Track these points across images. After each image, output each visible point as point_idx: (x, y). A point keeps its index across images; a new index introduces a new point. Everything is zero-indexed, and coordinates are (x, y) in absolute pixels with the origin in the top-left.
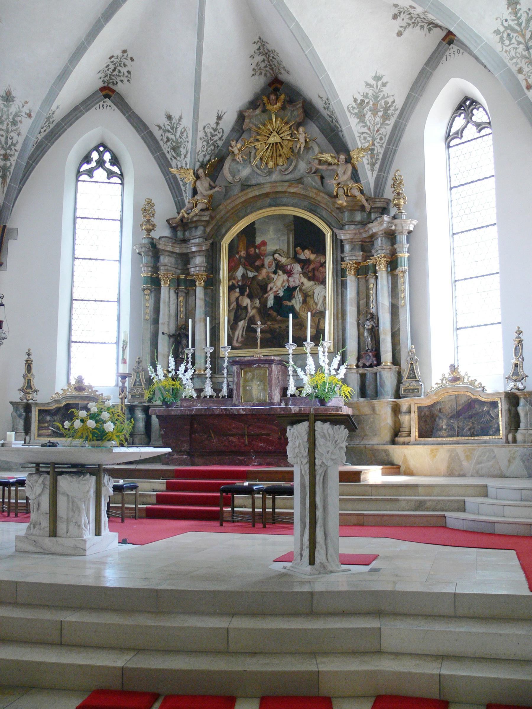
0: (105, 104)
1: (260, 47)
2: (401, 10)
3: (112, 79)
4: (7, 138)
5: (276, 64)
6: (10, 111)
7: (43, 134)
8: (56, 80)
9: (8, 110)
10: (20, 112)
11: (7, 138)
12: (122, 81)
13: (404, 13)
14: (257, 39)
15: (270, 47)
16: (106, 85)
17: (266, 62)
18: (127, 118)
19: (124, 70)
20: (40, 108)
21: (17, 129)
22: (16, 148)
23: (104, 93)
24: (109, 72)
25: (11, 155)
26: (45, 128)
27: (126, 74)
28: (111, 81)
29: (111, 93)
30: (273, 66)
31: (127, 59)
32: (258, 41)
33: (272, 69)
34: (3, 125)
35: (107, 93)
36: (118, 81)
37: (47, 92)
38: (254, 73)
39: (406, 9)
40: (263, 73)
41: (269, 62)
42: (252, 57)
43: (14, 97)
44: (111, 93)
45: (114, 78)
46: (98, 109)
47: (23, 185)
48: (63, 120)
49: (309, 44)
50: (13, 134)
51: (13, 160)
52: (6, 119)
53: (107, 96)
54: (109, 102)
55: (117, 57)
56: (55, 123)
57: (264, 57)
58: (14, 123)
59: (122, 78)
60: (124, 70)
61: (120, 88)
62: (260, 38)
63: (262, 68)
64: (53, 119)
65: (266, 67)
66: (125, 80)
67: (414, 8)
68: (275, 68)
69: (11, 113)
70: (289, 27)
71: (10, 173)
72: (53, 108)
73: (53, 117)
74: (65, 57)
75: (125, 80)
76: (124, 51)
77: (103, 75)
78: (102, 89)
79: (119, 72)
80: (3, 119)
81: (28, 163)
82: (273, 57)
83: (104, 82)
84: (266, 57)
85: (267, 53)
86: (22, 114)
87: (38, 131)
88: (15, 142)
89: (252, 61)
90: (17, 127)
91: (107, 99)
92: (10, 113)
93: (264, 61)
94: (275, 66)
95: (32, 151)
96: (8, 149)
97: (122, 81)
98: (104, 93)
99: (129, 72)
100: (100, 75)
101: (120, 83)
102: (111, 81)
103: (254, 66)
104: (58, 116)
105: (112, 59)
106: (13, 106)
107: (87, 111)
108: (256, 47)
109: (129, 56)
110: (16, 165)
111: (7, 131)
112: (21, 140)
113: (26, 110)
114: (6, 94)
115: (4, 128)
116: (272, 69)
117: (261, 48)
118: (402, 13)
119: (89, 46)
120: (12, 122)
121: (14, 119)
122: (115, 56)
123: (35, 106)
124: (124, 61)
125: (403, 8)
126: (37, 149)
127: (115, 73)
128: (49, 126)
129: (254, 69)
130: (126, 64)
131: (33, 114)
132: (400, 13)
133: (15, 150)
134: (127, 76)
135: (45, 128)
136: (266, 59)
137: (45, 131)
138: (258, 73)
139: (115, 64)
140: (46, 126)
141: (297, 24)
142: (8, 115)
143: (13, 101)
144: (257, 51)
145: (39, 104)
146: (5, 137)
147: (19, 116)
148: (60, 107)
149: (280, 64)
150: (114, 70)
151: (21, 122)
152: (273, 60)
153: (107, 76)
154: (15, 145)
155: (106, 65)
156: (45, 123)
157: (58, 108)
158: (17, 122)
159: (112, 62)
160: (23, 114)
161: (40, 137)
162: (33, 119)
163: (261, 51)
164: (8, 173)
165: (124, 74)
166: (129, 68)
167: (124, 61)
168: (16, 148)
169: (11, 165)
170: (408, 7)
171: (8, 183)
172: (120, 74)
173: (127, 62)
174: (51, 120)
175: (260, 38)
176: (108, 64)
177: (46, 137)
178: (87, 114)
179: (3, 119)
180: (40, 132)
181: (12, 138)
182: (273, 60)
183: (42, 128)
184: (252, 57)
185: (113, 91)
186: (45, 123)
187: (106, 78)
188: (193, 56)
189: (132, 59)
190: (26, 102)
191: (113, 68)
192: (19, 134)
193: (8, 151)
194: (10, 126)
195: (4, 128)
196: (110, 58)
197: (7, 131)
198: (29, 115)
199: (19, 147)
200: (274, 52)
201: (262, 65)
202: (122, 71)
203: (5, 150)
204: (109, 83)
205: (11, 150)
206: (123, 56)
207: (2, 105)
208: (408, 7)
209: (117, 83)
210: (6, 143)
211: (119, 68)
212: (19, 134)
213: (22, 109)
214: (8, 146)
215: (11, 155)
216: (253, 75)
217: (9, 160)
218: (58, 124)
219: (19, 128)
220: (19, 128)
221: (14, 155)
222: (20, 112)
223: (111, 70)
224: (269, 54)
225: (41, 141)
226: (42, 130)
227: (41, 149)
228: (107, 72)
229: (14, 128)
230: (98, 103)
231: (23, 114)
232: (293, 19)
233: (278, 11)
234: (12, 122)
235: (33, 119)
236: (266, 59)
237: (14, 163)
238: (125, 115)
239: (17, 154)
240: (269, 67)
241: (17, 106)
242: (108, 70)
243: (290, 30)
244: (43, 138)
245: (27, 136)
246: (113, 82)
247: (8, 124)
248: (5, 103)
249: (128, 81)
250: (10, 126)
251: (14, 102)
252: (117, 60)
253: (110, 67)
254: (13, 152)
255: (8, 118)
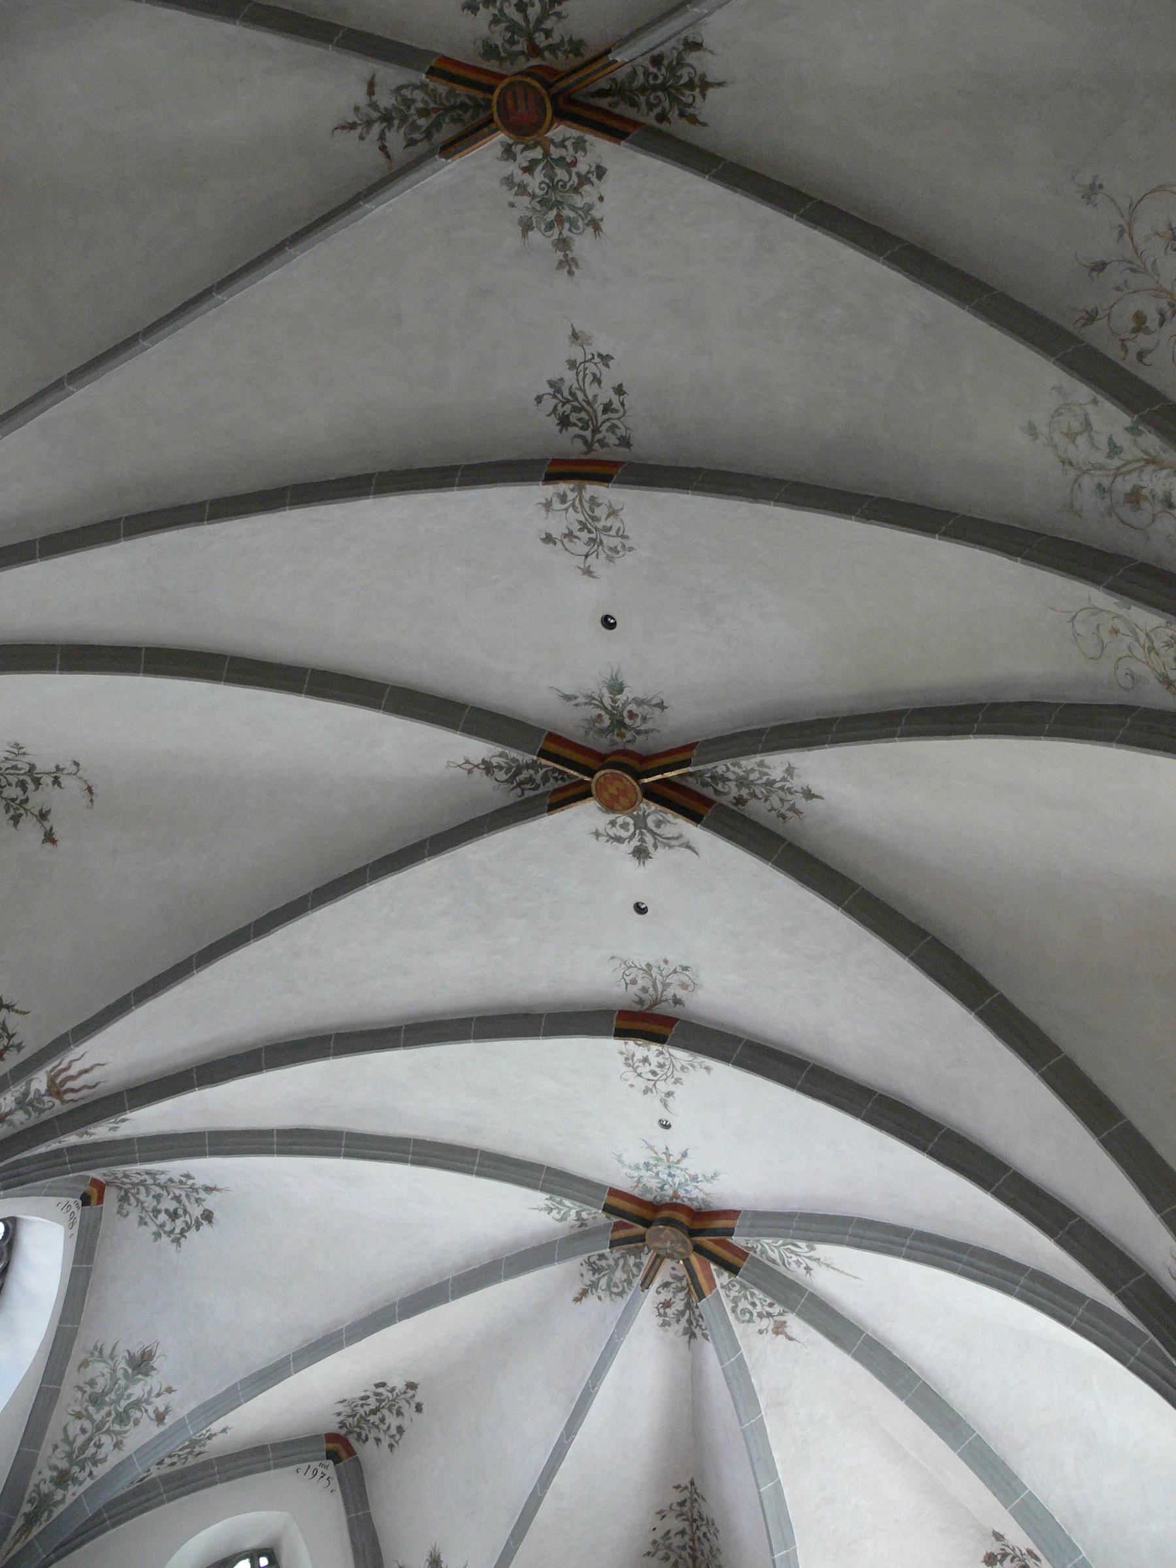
0: (320, 1470)
1: (685, 1501)
2: (1008, 1550)
3: (361, 1428)
4: (90, 1440)
5: (707, 1552)
6: (129, 1391)
7: (165, 1470)
8: (251, 1376)
9: (126, 1388)
10: (148, 1402)
11: (90, 1440)
12: (378, 1440)
13: (1012, 1561)
14: (685, 1482)
15: (709, 1509)
16: (343, 1432)
17: (687, 1538)
18: (349, 1520)
19: (393, 1421)
20: (190, 1415)
21: (118, 1433)
22: (94, 1469)
23: (331, 1446)
24: (361, 1411)
25: (75, 1481)
26: (175, 1459)
27: (393, 1431)
28: (357, 1430)
29: (343, 1454)
30: (699, 1554)
31: (408, 1402)
32: (686, 1488)
33: (694, 1558)
34: (98, 1411)
35: (341, 1449)
36: (371, 1437)
37: (220, 1391)
38: (652, 1550)
39: (1018, 1553)
40: (673, 1559)
41: (693, 1540)
42: (662, 1514)
43: (153, 1368)
44: (343, 1454)
45: (365, 1427)
46: (302, 1472)
47: (58, 1558)
48: (222, 1460)
49: (788, 1540)
50: (105, 1439)
51: (73, 1492)
52: (113, 1402)
53: (333, 1456)
54: (330, 1469)
55: (393, 1390)
56: (201, 1459)
57: (685, 1525)
58: (123, 1418)
59: (381, 1435)
60: (393, 1421)
61: (367, 1452)
62: (692, 1483)
63: (674, 1546)
64: (202, 1449)
65: (683, 1548)
66: (386, 1441)
67: (1037, 1558)
68: (701, 1558)
69: (129, 1396)
70: (758, 1488)
71: (50, 1515)
72: (216, 1427)
73: (204, 1445)
74: (296, 1342)
75: (386, 1441)
76: (412, 1386)
77: (348, 1410)
78: (331, 1437)
79: (383, 1420)
80: (107, 1399)
81: (98, 1514)
82: (705, 1534)
83: (342, 1425)
84: (691, 1525)
85: (695, 1520)
86: (148, 1407)
87: (157, 1459)
88: (100, 1456)
89: (658, 1524)
90: (124, 1428)
91: (331, 1462)
92: (126, 1393)
93: (682, 1533)
94: (703, 1554)
95: (122, 1492)
96: (77, 1464)
97: (378, 1440)
98: (331, 1446)
99: (400, 1430)
100: (340, 1408)
101: (371, 1443)
102: (357, 1430)
103: (658, 1535)
104: (215, 1447)
105: (380, 1390)
106: (142, 1383)
107: (276, 1466)
108: (678, 1497)
109: (417, 1399)
110: (71, 1505)
111: (98, 1428)
112: (114, 1458)
113: (160, 1403)
114: (143, 1355)
115: (97, 1418)
116: (694, 1558)
117: (688, 1504)
118: (1009, 1558)
119: (454, 1298)
120: (118, 1414)
121: (126, 1411)
122: (390, 1385)
123: (182, 1406)
124: (403, 1404)
125: (1013, 1550)
126: (134, 1494)
127: (372, 1418)
128: (186, 1458)
129: (654, 1542)
130: (403, 1410)
131: (169, 1420)
132: (1005, 1556)
133: (91, 1473)
134: (393, 1437)
135: (175, 1459)
136: (688, 1530)
137: (173, 1464)
138: (661, 1554)
139: (380, 1401)
140: (179, 1456)
141: (778, 1488)
142: (120, 1397)
143: (147, 1375)
144: (675, 1507)
145: (193, 1405)
146: (88, 1435)
147: (140, 1410)
148: (229, 1432)
149: (714, 1557)
150: (374, 1412)
151: (137, 1422)
152: (703, 1539)
153: (354, 1416)
154: (95, 1464)
155: (363, 1394)
156: (181, 1450)
157: (224, 1430)
158: (129, 1418)
159: (376, 1394)
160: (151, 1409)
161: (155, 1472)
162: (162, 1428)
163: (685, 1509)
164: (46, 1514)
165: (389, 1428)
166: (405, 1422)
167: (403, 1404)
168: (94, 1469)
169: (63, 1500)
170: (1024, 1551)
171: (31, 1537)
172: (381, 1426)
173: (406, 1409)
174: (197, 1449)
175: (692, 1483)
176: (368, 1394)
177: (167, 1479)
178: (273, 1472)
179: (107, 1399)
180: (161, 1463)
181: (99, 1446)
182: (703, 1539)
183: (170, 1456)
184: (662, 1514)
185: (351, 1452)
186: (181, 1450)
187: (351, 1420)
188: (541, 1458)
189: (419, 1408)
190: (170, 1390)
191: (372, 1407)
192: (118, 1445)
193: (76, 1469)
194: (111, 1419)
195: (97, 1418)
196: (377, 1386)
197: (98, 1428)
198: (160, 1418)
199: (100, 1471)
200: (710, 1523)
201: (677, 1541)
202: (387, 1422)
203: (72, 1463)
204: (350, 1432)
205: (83, 1468)
206: (405, 1393)
207: (122, 1371)
208: (1024, 1551)
209: (367, 1439)
210: (83, 1448)
211: (385, 1412)
212: (118, 1445)
213: (153, 1400)
214: (82, 1457)
215: (75, 1481)
216: (649, 1553)
217: (66, 1489)
218: (207, 1464)
219: (125, 1432)
220: (125, 1432)
221: (81, 1483)
222: (148, 1402)
223: (367, 1409)
224: (699, 1523)
225: (153, 1481)
226: (168, 1461)
227: (145, 1496)
228: (359, 1408)
229: (117, 1428)
230: (305, 1461)
231: (151, 1409)
232: (772, 1473)
233: (747, 1445)
234: (118, 1414)
235: (162, 1428)
236: (688, 1530)
237: (70, 1499)
238: (348, 1512)
239: (89, 1483)
240: (689, 1551)
241: (147, 1389)
242: (362, 1406)
243: (759, 1493)
244: (160, 1477)
245: (130, 1457)
246: (359, 1434)
247: (109, 1414)
248: (130, 1371)
249: (391, 1446)
250: (111, 1419)
251: (148, 1379)
252: (390, 1395)
253: (369, 1401)
254: (81, 1476)
255: (116, 1402)
